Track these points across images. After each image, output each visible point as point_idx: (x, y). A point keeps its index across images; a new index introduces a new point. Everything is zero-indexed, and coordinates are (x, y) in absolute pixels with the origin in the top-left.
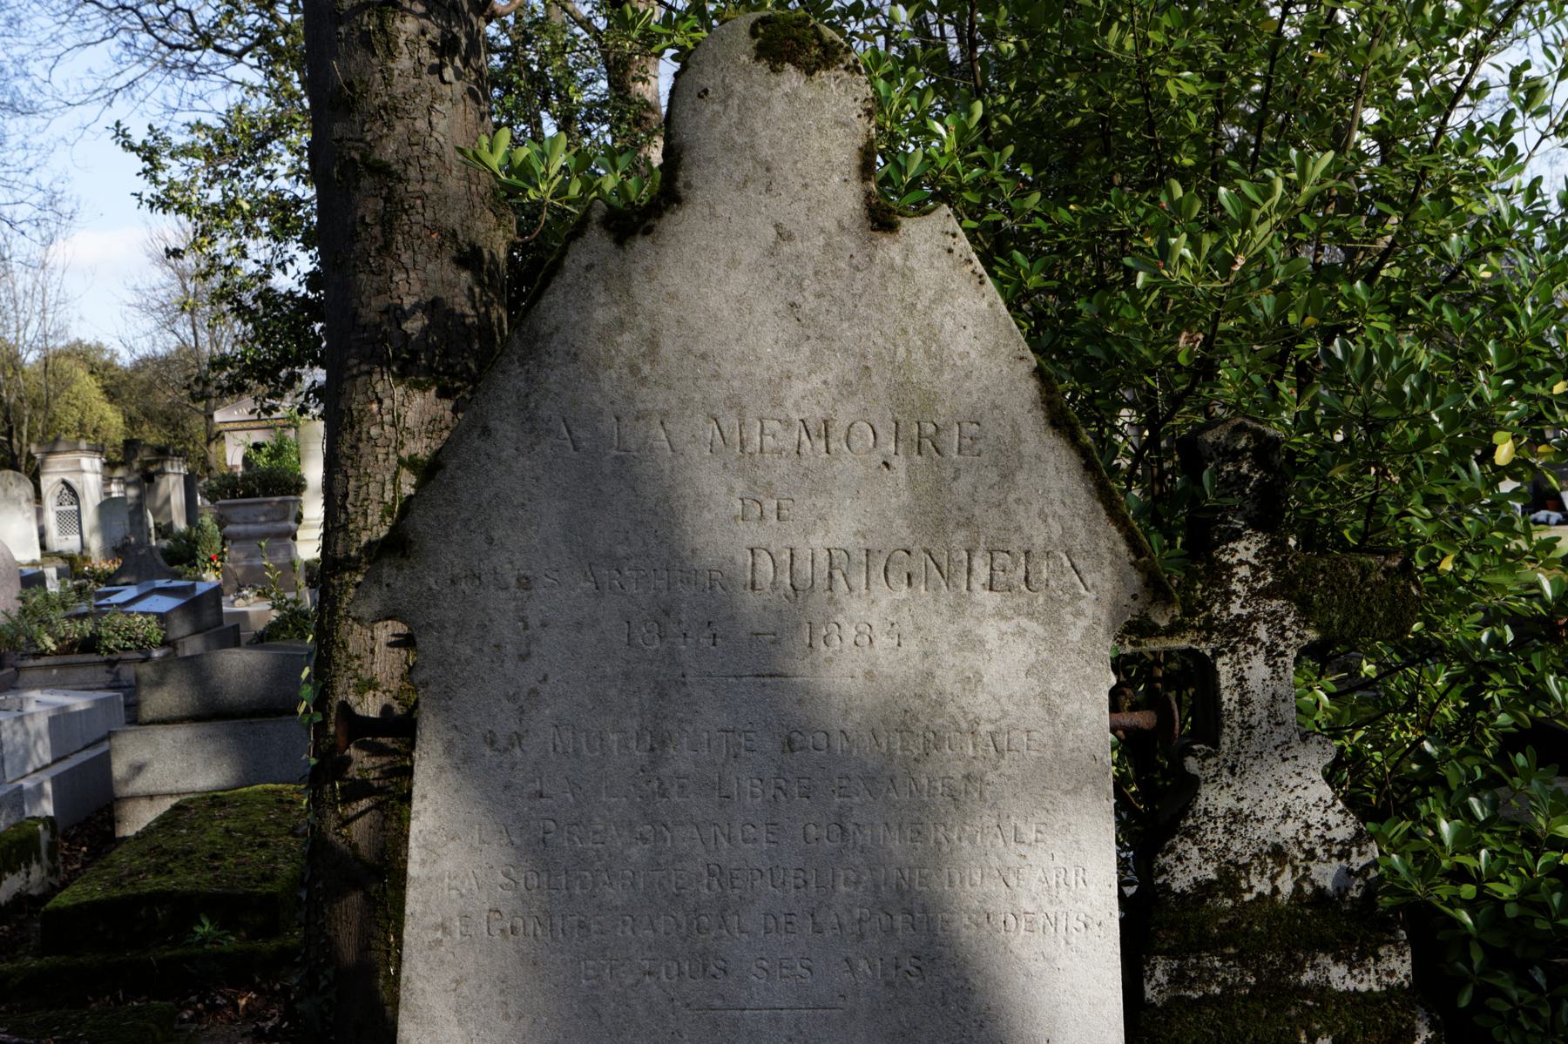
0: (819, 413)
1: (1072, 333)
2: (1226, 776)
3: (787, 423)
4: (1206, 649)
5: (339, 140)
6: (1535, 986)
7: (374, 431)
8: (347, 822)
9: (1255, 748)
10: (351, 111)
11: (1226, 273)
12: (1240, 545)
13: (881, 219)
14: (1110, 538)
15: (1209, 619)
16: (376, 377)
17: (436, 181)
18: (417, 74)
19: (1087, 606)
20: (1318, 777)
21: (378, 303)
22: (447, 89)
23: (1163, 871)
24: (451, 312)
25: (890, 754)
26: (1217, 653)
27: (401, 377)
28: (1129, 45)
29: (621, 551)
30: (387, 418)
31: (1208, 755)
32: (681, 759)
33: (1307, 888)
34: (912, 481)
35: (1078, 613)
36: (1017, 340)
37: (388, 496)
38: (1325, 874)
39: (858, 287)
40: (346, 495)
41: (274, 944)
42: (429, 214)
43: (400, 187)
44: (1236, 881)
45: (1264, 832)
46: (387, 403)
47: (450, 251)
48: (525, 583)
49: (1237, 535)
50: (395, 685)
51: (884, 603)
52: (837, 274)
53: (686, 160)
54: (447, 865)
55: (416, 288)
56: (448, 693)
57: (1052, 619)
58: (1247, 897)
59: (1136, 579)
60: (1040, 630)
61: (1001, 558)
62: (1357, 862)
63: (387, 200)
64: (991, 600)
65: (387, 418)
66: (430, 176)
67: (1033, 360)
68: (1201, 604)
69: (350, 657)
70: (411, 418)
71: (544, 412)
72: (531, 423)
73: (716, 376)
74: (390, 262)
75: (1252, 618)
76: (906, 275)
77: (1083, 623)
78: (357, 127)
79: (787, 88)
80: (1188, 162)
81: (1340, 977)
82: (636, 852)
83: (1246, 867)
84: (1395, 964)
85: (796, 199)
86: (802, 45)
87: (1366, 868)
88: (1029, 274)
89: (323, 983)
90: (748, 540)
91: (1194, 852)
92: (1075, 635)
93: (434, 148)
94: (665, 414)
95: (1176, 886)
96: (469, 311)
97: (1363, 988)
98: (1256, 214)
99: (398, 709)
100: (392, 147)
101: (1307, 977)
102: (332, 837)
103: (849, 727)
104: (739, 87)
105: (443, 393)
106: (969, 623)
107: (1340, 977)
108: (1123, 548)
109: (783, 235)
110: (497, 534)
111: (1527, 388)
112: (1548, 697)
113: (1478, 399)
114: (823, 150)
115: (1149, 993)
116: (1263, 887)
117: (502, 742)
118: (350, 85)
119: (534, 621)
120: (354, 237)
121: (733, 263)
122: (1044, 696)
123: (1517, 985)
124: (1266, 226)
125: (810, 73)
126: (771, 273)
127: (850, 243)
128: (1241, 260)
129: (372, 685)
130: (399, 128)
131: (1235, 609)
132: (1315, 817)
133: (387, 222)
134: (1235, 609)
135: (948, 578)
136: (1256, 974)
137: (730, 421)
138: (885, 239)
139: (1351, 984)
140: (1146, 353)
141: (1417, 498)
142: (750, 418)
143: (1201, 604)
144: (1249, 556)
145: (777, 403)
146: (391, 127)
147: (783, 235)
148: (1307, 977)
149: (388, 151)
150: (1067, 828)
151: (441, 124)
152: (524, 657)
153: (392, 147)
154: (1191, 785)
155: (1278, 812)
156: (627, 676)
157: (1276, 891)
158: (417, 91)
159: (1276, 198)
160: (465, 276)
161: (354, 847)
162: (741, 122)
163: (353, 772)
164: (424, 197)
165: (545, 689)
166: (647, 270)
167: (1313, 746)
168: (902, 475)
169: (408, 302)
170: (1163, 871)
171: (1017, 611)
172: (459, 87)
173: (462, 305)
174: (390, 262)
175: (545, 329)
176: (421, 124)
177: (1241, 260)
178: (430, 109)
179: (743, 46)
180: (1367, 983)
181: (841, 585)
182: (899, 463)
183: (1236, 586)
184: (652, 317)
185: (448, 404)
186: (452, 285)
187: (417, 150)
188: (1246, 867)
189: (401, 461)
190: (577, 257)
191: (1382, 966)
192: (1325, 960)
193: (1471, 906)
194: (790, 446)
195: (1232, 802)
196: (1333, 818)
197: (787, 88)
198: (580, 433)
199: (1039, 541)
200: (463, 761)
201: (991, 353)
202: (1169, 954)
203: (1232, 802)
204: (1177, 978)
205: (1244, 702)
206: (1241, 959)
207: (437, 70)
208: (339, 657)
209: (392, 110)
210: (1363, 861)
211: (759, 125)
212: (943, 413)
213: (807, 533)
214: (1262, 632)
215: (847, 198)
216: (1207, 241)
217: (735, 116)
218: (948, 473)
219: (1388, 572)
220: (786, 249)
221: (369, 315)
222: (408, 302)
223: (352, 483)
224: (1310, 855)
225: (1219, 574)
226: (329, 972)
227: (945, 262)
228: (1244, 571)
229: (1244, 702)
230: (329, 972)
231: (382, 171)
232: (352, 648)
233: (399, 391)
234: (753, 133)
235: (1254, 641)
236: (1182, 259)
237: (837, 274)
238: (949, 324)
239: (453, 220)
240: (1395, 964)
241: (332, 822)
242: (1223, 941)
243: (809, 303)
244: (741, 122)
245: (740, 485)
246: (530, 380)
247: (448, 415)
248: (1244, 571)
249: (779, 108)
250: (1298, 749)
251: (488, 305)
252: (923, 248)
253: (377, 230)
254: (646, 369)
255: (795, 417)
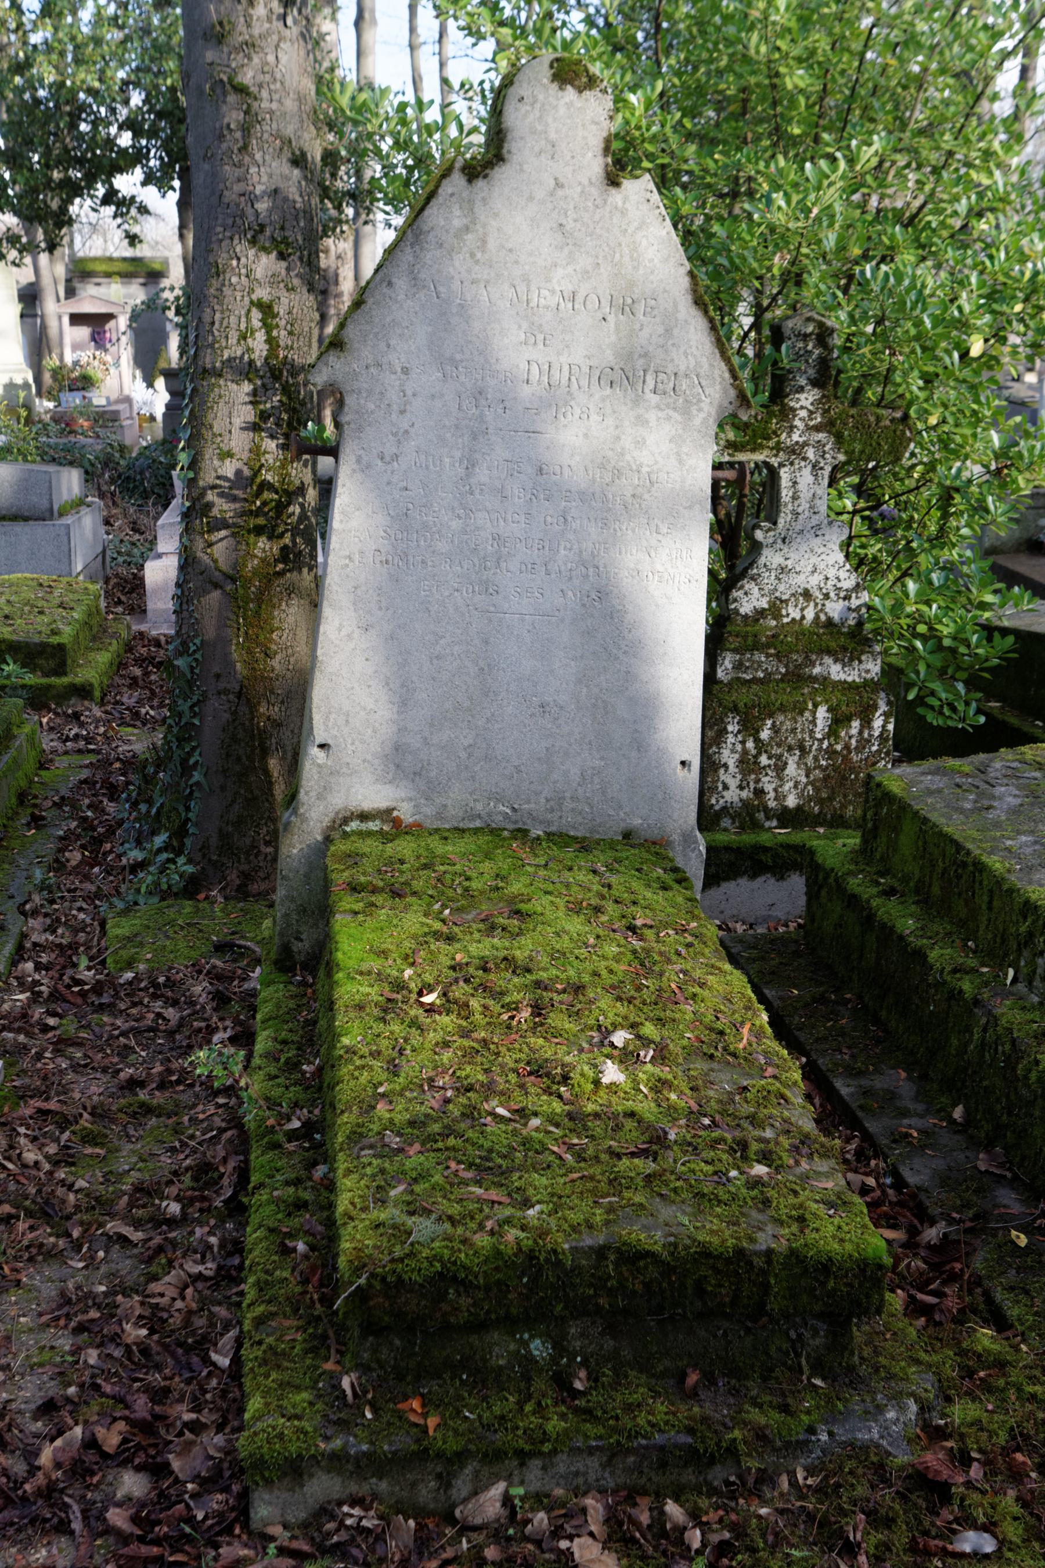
0: (571, 288)
1: (708, 248)
2: (779, 544)
3: (553, 292)
4: (774, 462)
5: (211, 64)
6: (957, 694)
7: (234, 280)
8: (210, 545)
9: (799, 527)
10: (220, 43)
11: (807, 218)
12: (802, 396)
13: (613, 181)
14: (721, 369)
15: (778, 443)
16: (236, 241)
17: (280, 101)
18: (269, 20)
19: (705, 406)
20: (837, 548)
21: (238, 188)
22: (287, 32)
23: (735, 600)
24: (286, 199)
25: (594, 481)
26: (781, 465)
27: (253, 242)
28: (763, 49)
29: (458, 357)
30: (243, 271)
31: (769, 530)
32: (482, 475)
33: (823, 617)
34: (617, 330)
35: (700, 410)
36: (678, 253)
37: (243, 326)
38: (835, 609)
39: (597, 217)
40: (213, 323)
41: (65, 680)
42: (274, 126)
43: (255, 104)
44: (779, 610)
45: (800, 581)
46: (243, 260)
47: (287, 154)
48: (405, 371)
49: (801, 390)
50: (245, 456)
51: (597, 396)
52: (586, 209)
53: (509, 137)
54: (354, 523)
55: (264, 179)
56: (360, 429)
57: (686, 412)
58: (785, 620)
59: (732, 393)
60: (679, 418)
61: (661, 376)
62: (855, 603)
63: (246, 113)
64: (654, 399)
65: (243, 271)
66: (276, 97)
67: (688, 266)
68: (775, 433)
69: (215, 435)
70: (259, 272)
71: (422, 276)
72: (415, 281)
73: (517, 262)
74: (247, 159)
75: (806, 444)
76: (623, 213)
77: (702, 415)
78: (225, 56)
79: (567, 100)
80: (797, 131)
81: (836, 672)
82: (455, 524)
83: (786, 601)
84: (870, 666)
85: (567, 164)
86: (577, 75)
87: (859, 608)
88: (684, 203)
89: (193, 648)
90: (527, 357)
91: (755, 590)
92: (697, 421)
93: (278, 76)
94: (488, 282)
95: (742, 611)
96: (298, 199)
97: (850, 679)
98: (826, 183)
99: (247, 472)
100: (250, 74)
101: (817, 670)
102: (200, 554)
103: (573, 464)
104: (541, 97)
105: (282, 256)
106: (641, 411)
107: (836, 672)
108: (727, 375)
109: (559, 185)
110: (393, 342)
111: (995, 306)
112: (987, 511)
113: (960, 309)
114: (584, 138)
115: (720, 674)
116: (795, 614)
117: (388, 459)
118: (221, 23)
119: (409, 393)
120: (221, 137)
121: (531, 198)
122: (678, 454)
123: (946, 691)
124: (832, 189)
125: (581, 92)
126: (550, 206)
127: (594, 192)
128: (815, 211)
129: (230, 454)
130: (256, 60)
131: (796, 437)
132: (832, 573)
133: (246, 130)
134: (796, 437)
135: (632, 385)
136: (786, 666)
137: (522, 288)
138: (613, 191)
139: (842, 676)
140: (755, 265)
141: (916, 373)
142: (533, 288)
143: (775, 433)
144: (807, 404)
145: (548, 280)
146: (250, 59)
147: (559, 185)
148: (817, 670)
149: (248, 77)
150: (683, 528)
151: (284, 59)
152: (402, 412)
153: (250, 74)
154: (756, 548)
155: (810, 568)
156: (457, 427)
157: (803, 617)
158: (269, 33)
159: (840, 172)
160: (296, 172)
161: (215, 561)
162: (541, 118)
163: (215, 512)
164: (271, 112)
165: (412, 430)
166: (484, 199)
167: (835, 529)
168: (612, 325)
169: (259, 189)
170: (735, 600)
171: (668, 406)
172: (295, 31)
173: (293, 194)
174: (247, 159)
175: (425, 228)
176: (271, 58)
177: (815, 211)
178: (277, 46)
179: (543, 71)
180: (852, 676)
181: (575, 385)
182: (611, 319)
183: (797, 422)
184: (484, 226)
185: (284, 264)
186: (288, 178)
187: (268, 77)
188: (786, 601)
189: (252, 302)
190: (447, 188)
191: (863, 666)
192: (828, 660)
193: (924, 638)
194: (554, 305)
195: (781, 560)
196: (843, 574)
197: (567, 100)
198: (441, 289)
199: (682, 368)
200: (364, 468)
201: (666, 260)
202: (735, 651)
203: (781, 560)
204: (738, 666)
205: (795, 497)
206: (778, 656)
207: (283, 17)
208: (208, 435)
209: (250, 46)
210: (858, 602)
211: (550, 120)
212: (637, 293)
213: (559, 354)
214: (811, 453)
215: (595, 165)
216: (795, 198)
217: (537, 114)
218: (637, 327)
219: (892, 420)
220: (560, 192)
221: (229, 196)
222: (259, 189)
223: (218, 316)
224: (827, 596)
225: (787, 414)
226: (197, 641)
227: (645, 207)
228: (803, 413)
229: (795, 497)
230: (197, 641)
231: (242, 90)
232: (216, 429)
233: (252, 253)
234: (547, 125)
235: (805, 459)
236: (779, 208)
237: (586, 209)
238: (644, 242)
239: (289, 131)
240: (870, 666)
241: (200, 544)
242: (768, 646)
243: (570, 225)
244: (541, 118)
245: (525, 325)
246: (416, 257)
247: (283, 272)
248: (803, 413)
249: (562, 111)
250: (826, 530)
251: (309, 195)
252: (634, 198)
253: (238, 135)
254: (479, 255)
255: (558, 288)
